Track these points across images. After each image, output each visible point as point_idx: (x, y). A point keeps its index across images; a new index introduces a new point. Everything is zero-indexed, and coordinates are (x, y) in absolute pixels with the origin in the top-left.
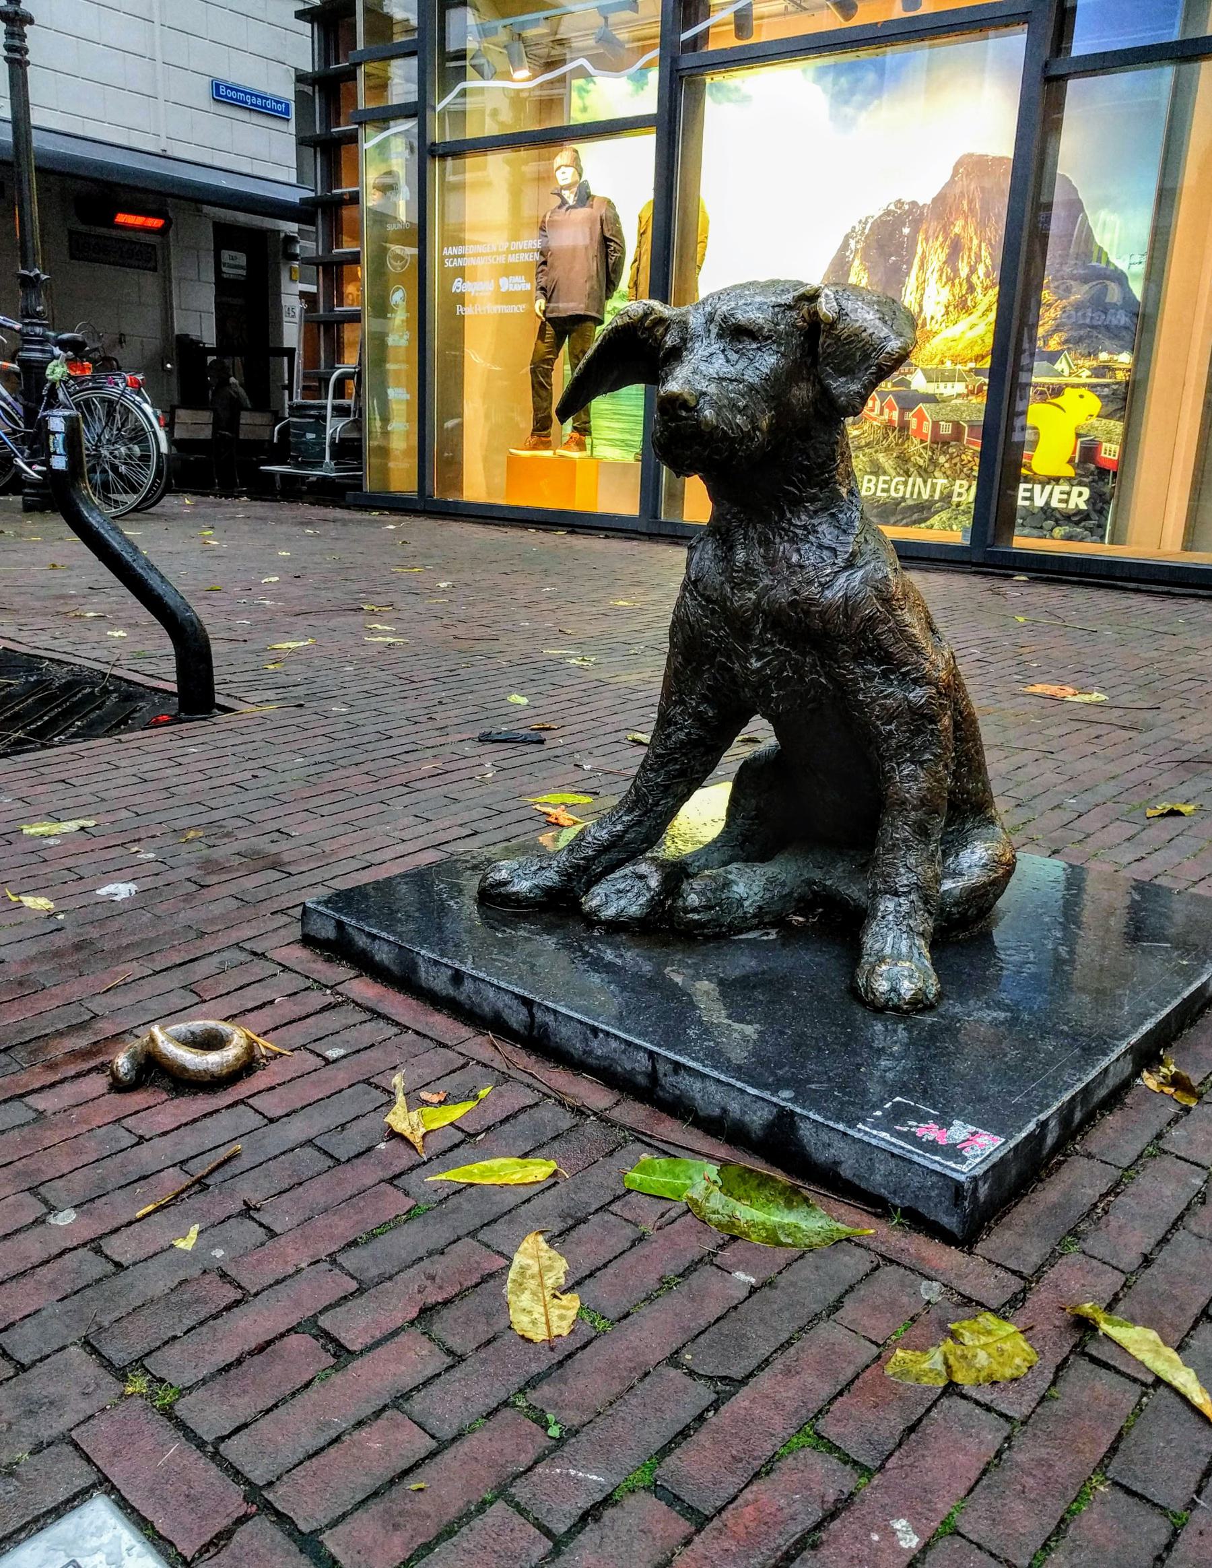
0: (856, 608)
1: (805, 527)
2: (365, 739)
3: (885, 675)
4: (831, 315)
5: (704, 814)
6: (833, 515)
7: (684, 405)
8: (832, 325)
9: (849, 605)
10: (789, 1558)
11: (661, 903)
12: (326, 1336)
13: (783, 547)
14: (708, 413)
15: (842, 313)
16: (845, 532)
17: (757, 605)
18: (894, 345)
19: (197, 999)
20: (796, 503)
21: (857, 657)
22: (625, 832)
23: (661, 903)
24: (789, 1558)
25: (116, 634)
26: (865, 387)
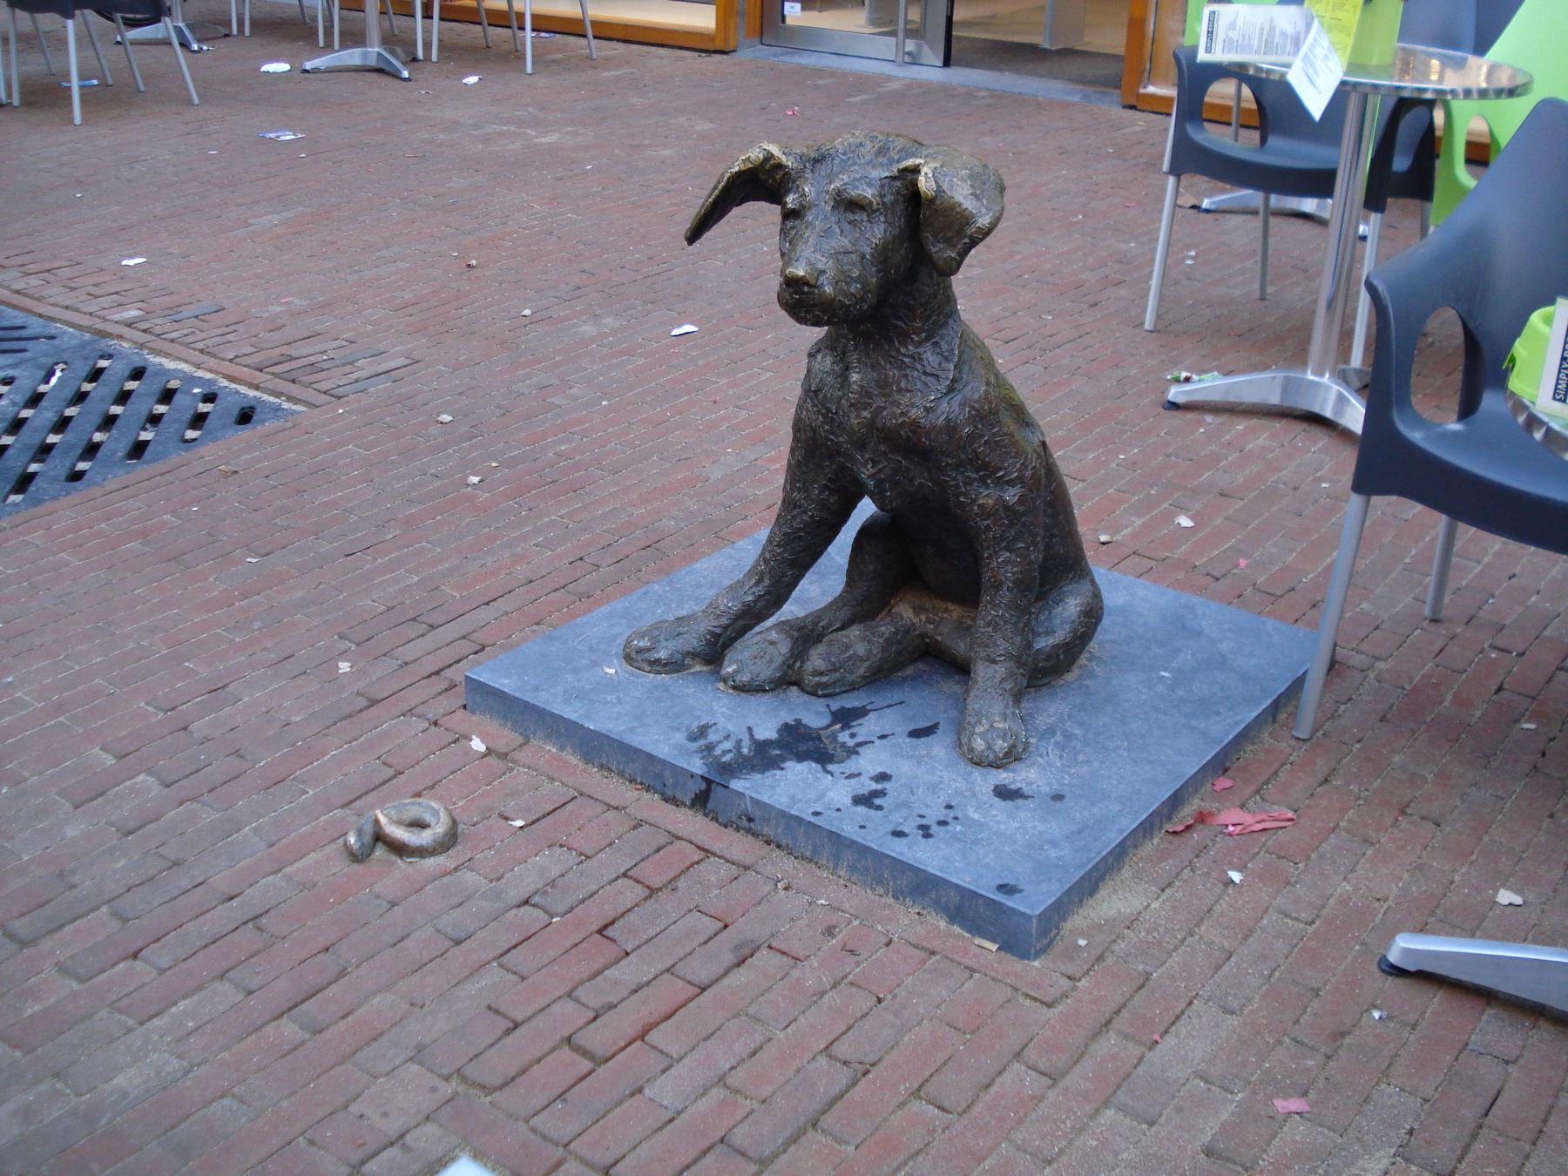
0: (955, 428)
1: (912, 357)
2: (393, 364)
3: (983, 480)
4: (931, 194)
5: (823, 584)
6: (935, 344)
7: (807, 284)
8: (932, 201)
9: (951, 427)
10: (682, 1172)
11: (790, 667)
12: (584, 1053)
13: (893, 373)
14: (828, 289)
15: (940, 190)
16: (946, 359)
17: (871, 425)
18: (984, 221)
19: (840, 1050)
20: (904, 336)
21: (959, 465)
22: (756, 602)
23: (790, 667)
24: (682, 1172)
25: (131, 262)
26: (959, 254)
